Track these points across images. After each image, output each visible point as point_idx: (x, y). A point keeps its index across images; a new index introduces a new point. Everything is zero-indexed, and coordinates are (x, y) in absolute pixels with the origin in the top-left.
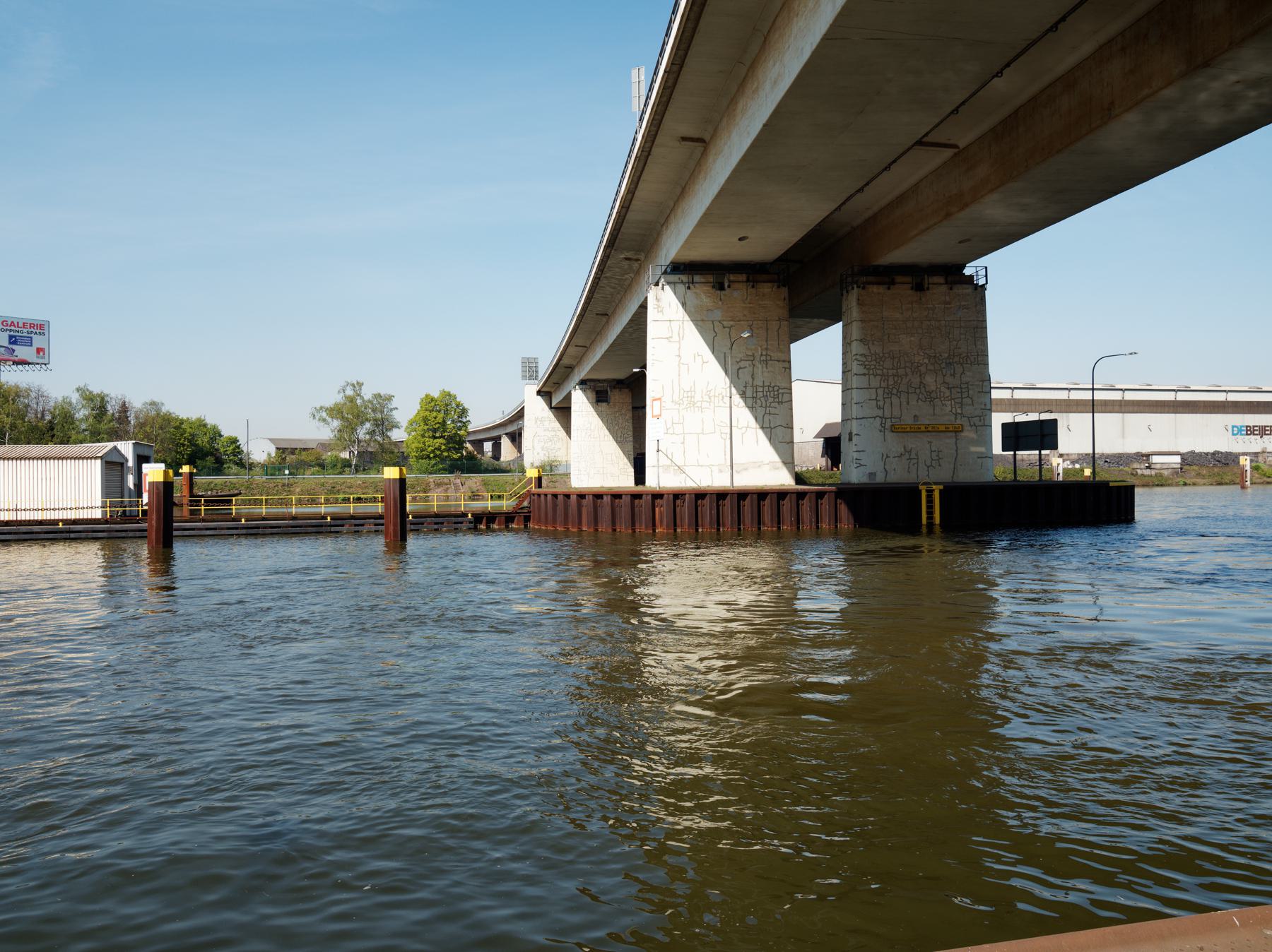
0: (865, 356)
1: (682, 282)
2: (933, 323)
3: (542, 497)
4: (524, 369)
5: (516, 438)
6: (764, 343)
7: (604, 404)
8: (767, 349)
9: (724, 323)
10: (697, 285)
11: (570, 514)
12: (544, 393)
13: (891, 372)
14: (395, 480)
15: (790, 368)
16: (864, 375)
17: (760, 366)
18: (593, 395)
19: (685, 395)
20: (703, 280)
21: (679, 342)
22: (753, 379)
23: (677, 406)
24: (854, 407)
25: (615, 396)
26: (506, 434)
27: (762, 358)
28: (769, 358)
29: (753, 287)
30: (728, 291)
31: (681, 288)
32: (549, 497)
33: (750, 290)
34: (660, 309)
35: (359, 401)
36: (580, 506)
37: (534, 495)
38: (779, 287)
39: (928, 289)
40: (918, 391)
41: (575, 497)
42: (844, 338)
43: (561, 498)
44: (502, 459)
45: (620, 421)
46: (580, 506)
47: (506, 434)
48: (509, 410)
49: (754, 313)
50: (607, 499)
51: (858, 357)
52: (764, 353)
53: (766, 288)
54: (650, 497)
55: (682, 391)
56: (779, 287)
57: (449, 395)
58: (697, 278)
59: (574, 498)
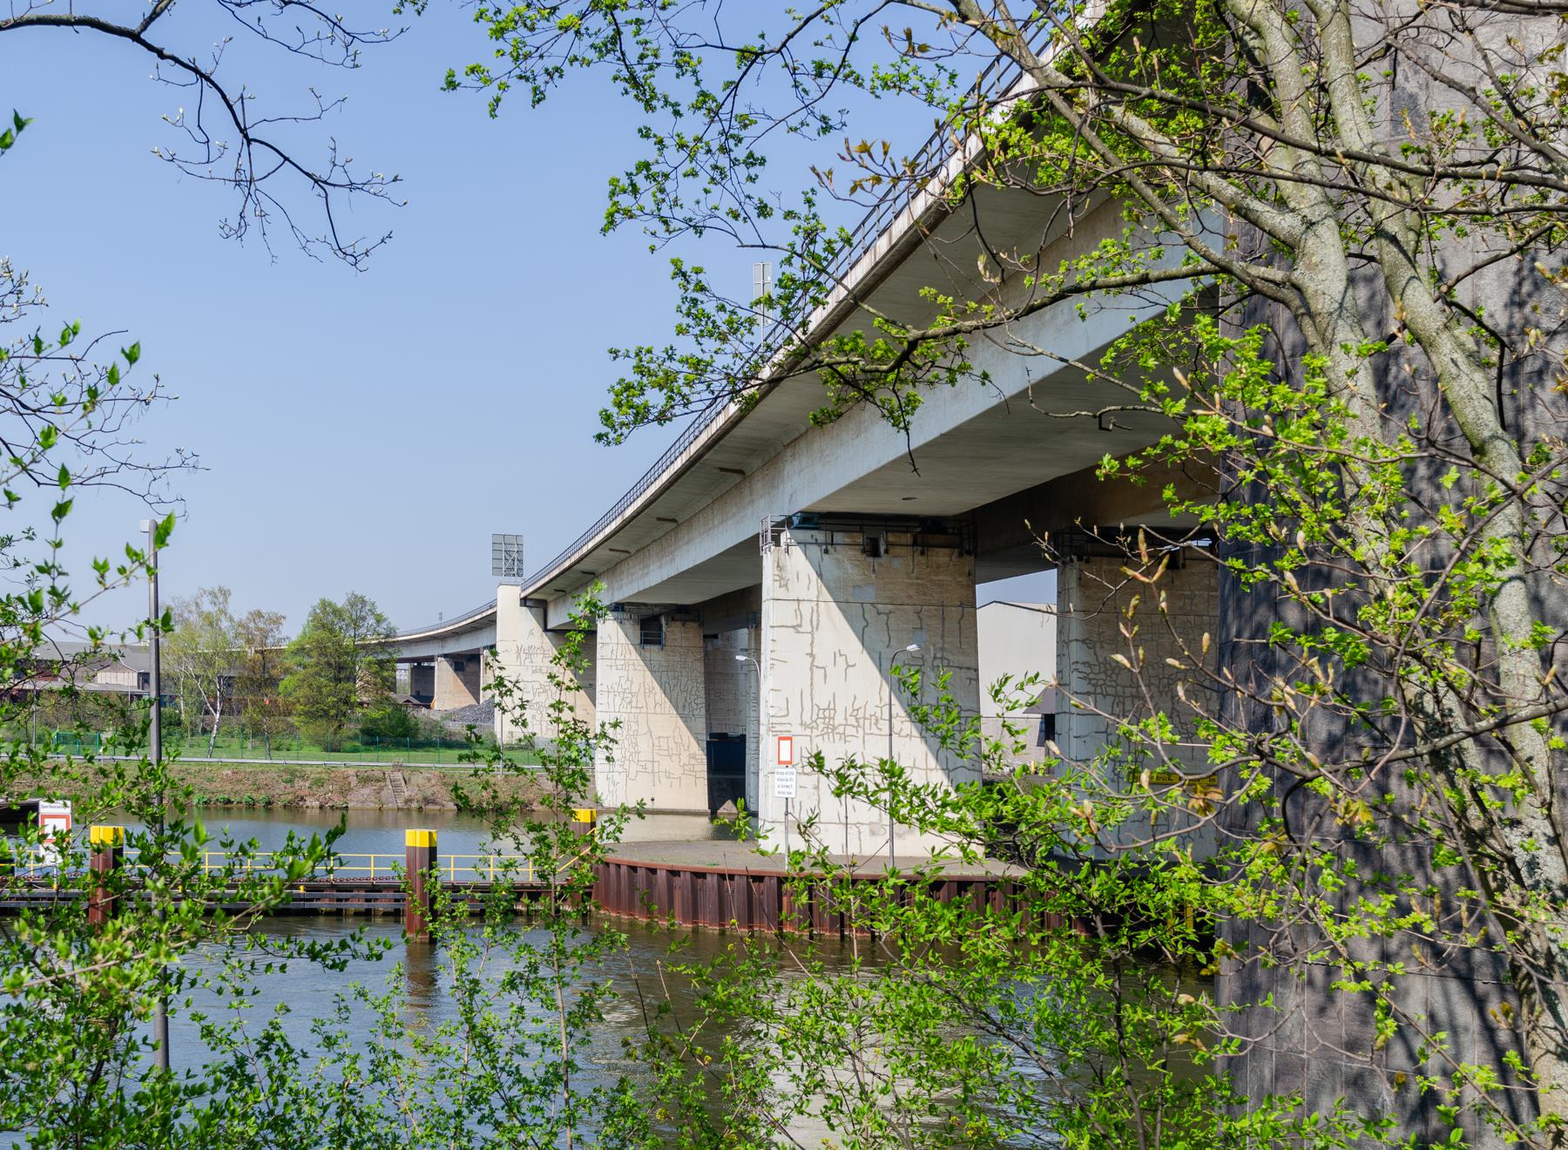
1: (816, 543)
2: (1191, 618)
3: (612, 868)
5: (465, 664)
7: (655, 648)
8: (943, 649)
9: (880, 607)
12: (537, 603)
13: (1128, 691)
14: (422, 849)
15: (977, 680)
16: (1088, 693)
18: (636, 632)
20: (848, 540)
21: (812, 633)
23: (808, 732)
24: (1073, 741)
25: (673, 632)
26: (445, 656)
29: (922, 553)
30: (884, 559)
31: (815, 551)
32: (624, 869)
33: (919, 558)
34: (783, 582)
35: (225, 624)
36: (670, 889)
37: (732, 877)
38: (961, 555)
39: (1184, 566)
42: (1060, 632)
43: (641, 872)
44: (436, 704)
45: (684, 680)
46: (670, 889)
47: (445, 656)
48: (457, 612)
49: (925, 594)
50: (711, 881)
53: (942, 556)
54: (775, 881)
56: (961, 555)
57: (363, 602)
58: (839, 537)
59: (662, 875)
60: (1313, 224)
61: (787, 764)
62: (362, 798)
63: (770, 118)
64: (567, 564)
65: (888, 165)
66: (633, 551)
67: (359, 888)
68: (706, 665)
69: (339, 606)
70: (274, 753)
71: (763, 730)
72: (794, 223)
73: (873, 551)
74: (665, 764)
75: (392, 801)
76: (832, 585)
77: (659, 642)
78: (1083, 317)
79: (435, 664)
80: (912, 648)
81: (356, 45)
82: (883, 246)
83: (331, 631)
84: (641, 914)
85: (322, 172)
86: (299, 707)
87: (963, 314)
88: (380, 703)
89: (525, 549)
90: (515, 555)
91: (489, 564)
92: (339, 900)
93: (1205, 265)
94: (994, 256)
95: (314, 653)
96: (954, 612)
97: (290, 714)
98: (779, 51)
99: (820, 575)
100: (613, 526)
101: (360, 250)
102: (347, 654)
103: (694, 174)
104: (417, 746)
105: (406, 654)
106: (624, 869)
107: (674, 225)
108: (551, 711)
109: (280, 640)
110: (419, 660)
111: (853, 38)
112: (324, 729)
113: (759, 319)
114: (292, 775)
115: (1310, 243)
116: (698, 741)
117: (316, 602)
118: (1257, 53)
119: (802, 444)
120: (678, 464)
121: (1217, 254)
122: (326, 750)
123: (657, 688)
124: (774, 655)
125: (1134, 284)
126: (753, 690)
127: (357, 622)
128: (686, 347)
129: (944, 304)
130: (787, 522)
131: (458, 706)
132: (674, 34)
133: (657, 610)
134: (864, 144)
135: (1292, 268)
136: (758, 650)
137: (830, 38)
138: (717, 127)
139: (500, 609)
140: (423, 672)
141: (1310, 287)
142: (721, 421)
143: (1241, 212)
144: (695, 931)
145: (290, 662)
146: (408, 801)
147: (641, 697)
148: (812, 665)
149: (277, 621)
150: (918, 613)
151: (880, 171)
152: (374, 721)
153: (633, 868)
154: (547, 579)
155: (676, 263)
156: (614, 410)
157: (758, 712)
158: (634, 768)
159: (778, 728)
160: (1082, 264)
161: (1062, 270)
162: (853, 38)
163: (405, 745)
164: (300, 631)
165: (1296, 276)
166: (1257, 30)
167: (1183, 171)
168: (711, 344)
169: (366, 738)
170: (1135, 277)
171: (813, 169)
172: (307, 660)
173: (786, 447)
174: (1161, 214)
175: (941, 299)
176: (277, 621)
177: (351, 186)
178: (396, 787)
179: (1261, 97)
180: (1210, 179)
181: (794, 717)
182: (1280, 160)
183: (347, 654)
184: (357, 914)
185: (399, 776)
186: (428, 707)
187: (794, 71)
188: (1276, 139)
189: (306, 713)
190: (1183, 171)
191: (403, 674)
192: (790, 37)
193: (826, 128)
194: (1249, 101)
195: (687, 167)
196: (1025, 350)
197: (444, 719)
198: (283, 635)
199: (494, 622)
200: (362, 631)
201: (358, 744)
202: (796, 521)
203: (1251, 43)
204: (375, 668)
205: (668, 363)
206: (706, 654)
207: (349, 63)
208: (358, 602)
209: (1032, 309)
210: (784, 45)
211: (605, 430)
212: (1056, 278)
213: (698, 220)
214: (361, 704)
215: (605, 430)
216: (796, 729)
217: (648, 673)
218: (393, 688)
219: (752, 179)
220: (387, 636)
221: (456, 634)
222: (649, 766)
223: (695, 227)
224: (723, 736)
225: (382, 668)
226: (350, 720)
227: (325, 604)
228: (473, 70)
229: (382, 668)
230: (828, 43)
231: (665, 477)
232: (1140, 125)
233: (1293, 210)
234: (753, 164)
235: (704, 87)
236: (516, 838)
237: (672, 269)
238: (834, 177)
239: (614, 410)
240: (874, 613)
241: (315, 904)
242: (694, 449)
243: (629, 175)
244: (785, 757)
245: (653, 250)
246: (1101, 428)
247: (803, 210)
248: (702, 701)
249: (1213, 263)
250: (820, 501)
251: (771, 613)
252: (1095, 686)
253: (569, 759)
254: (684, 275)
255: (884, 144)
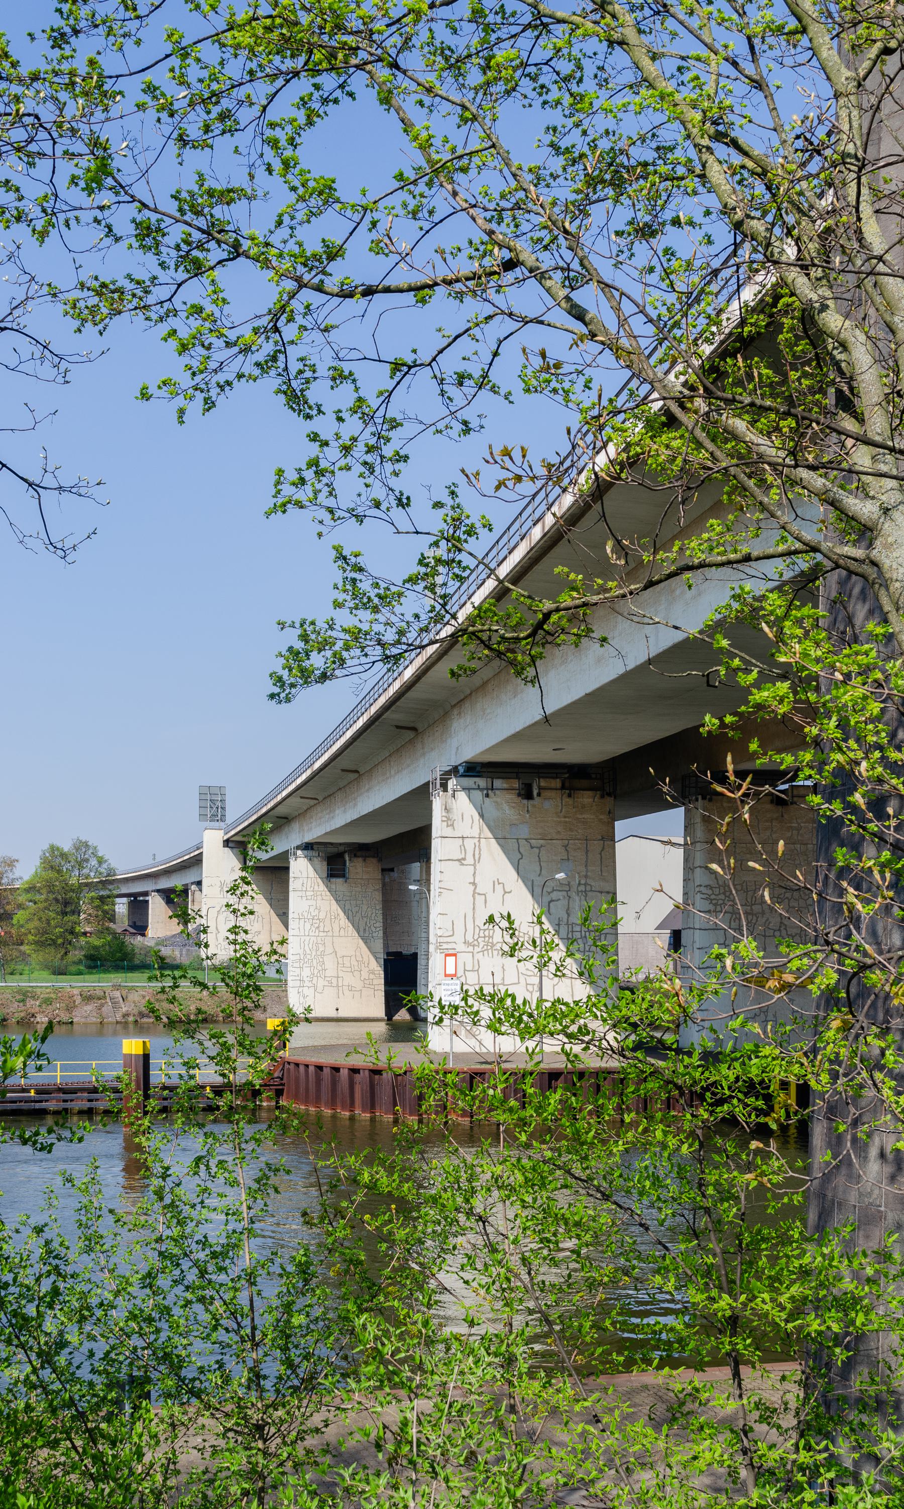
0: (711, 888)
1: (479, 788)
3: (302, 1068)
4: (203, 797)
6: (583, 868)
7: (340, 881)
8: (586, 877)
9: (533, 842)
10: (497, 792)
11: (339, 1092)
17: (577, 898)
19: (482, 934)
20: (505, 786)
21: (474, 865)
22: (568, 915)
23: (471, 949)
24: (697, 952)
25: (355, 867)
26: (158, 891)
27: (582, 888)
28: (588, 888)
29: (569, 796)
30: (537, 801)
31: (478, 795)
32: (311, 1069)
33: (566, 800)
37: (289, 1063)
38: (602, 797)
40: (777, 933)
41: (346, 1071)
42: (686, 860)
43: (327, 1071)
44: (150, 932)
45: (365, 907)
47: (158, 891)
49: (571, 830)
51: (702, 889)
52: (583, 882)
53: (586, 798)
55: (477, 930)
56: (602, 797)
57: (86, 845)
58: (498, 783)
59: (344, 1073)
60: (888, 510)
61: (452, 976)
62: (85, 1014)
63: (421, 422)
64: (264, 810)
65: (526, 466)
66: (320, 798)
67: (82, 1090)
68: (384, 894)
69: (66, 850)
70: (8, 977)
71: (432, 948)
72: (441, 512)
73: (527, 794)
74: (348, 979)
75: (111, 1015)
76: (492, 824)
77: (343, 876)
78: (690, 587)
79: (149, 898)
80: (561, 876)
81: (64, 365)
82: (537, 533)
83: (59, 872)
84: (326, 1106)
85: (35, 478)
86: (31, 937)
87: (589, 589)
88: (100, 933)
89: (227, 798)
90: (219, 804)
91: (196, 811)
92: (65, 1101)
93: (798, 545)
94: (619, 542)
95: (44, 891)
96: (596, 846)
97: (22, 944)
98: (430, 364)
99: (482, 816)
100: (304, 777)
101: (68, 544)
102: (73, 891)
103: (348, 468)
104: (133, 968)
105: (124, 890)
106: (311, 1069)
107: (339, 513)
108: (228, 934)
109: (13, 880)
110: (135, 895)
111: (496, 354)
112: (53, 955)
113: (407, 593)
114: (24, 995)
115: (886, 526)
116: (376, 958)
117: (46, 847)
118: (843, 365)
119: (467, 704)
120: (360, 723)
121: (807, 536)
122: (54, 973)
123: (342, 914)
124: (442, 885)
125: (738, 562)
126: (424, 915)
127: (81, 864)
128: (345, 619)
129: (575, 581)
130: (454, 771)
131: (169, 933)
132: (336, 348)
133: (342, 849)
134: (506, 448)
135: (870, 546)
136: (428, 881)
137: (476, 353)
138: (371, 429)
139: (205, 850)
140: (138, 905)
141: (886, 563)
142: (397, 685)
143: (833, 503)
144: (373, 1120)
145: (22, 898)
146: (126, 1015)
147: (327, 922)
148: (474, 892)
149: (11, 863)
150: (566, 846)
151: (520, 472)
152: (96, 948)
153: (320, 1068)
154: (246, 823)
155: (338, 549)
156: (285, 674)
157: (428, 933)
158: (321, 983)
159: (445, 946)
160: (693, 545)
161: (675, 548)
162: (496, 354)
163: (123, 968)
164: (32, 871)
165: (874, 554)
166: (844, 346)
167: (780, 468)
168: (365, 615)
169: (90, 963)
170: (738, 556)
171: (463, 471)
172: (37, 897)
173: (453, 707)
174: (761, 503)
175: (572, 576)
176: (11, 863)
177: (60, 488)
178: (115, 1003)
179: (846, 403)
180: (803, 473)
181: (459, 937)
182: (862, 457)
183: (73, 891)
184: (81, 1113)
185: (117, 994)
186: (143, 935)
187: (441, 382)
188: (857, 440)
189: (36, 943)
190: (780, 468)
191: (121, 907)
192: (441, 352)
193: (467, 428)
194: (837, 405)
195: (342, 463)
196: (646, 620)
197: (157, 944)
198: (17, 875)
199: (201, 861)
200: (85, 871)
201: (82, 968)
202: (461, 770)
203: (839, 357)
204: (97, 902)
205: (329, 633)
206: (384, 885)
207: (60, 379)
208: (82, 846)
209: (650, 584)
210: (434, 359)
211: (277, 690)
212: (668, 558)
213: (360, 511)
214: (85, 934)
215: (277, 690)
216: (460, 947)
217: (334, 902)
218: (112, 919)
219: (396, 474)
220: (108, 875)
221: (167, 872)
222: (334, 981)
223: (356, 516)
224: (398, 954)
225: (103, 903)
226: (75, 948)
227: (53, 848)
228: (164, 383)
229: (103, 903)
230: (475, 358)
231: (349, 734)
232: (740, 425)
233: (873, 498)
234: (398, 461)
235: (362, 393)
236: (201, 1044)
237: (334, 553)
238: (480, 477)
239: (285, 674)
240: (528, 847)
241: (43, 1105)
242: (373, 710)
243: (299, 470)
244: (451, 970)
245: (320, 535)
246: (708, 685)
247: (449, 501)
248: (380, 924)
249: (804, 544)
250: (482, 753)
251: (439, 849)
252: (715, 905)
253: (244, 974)
254: (345, 558)
255: (522, 449)
